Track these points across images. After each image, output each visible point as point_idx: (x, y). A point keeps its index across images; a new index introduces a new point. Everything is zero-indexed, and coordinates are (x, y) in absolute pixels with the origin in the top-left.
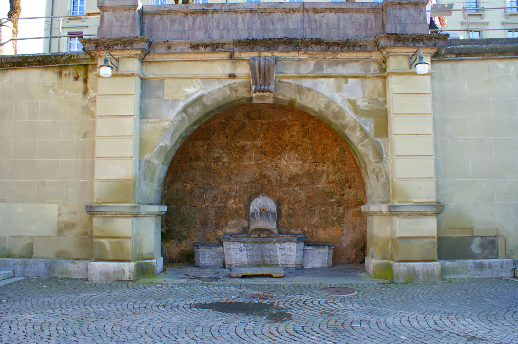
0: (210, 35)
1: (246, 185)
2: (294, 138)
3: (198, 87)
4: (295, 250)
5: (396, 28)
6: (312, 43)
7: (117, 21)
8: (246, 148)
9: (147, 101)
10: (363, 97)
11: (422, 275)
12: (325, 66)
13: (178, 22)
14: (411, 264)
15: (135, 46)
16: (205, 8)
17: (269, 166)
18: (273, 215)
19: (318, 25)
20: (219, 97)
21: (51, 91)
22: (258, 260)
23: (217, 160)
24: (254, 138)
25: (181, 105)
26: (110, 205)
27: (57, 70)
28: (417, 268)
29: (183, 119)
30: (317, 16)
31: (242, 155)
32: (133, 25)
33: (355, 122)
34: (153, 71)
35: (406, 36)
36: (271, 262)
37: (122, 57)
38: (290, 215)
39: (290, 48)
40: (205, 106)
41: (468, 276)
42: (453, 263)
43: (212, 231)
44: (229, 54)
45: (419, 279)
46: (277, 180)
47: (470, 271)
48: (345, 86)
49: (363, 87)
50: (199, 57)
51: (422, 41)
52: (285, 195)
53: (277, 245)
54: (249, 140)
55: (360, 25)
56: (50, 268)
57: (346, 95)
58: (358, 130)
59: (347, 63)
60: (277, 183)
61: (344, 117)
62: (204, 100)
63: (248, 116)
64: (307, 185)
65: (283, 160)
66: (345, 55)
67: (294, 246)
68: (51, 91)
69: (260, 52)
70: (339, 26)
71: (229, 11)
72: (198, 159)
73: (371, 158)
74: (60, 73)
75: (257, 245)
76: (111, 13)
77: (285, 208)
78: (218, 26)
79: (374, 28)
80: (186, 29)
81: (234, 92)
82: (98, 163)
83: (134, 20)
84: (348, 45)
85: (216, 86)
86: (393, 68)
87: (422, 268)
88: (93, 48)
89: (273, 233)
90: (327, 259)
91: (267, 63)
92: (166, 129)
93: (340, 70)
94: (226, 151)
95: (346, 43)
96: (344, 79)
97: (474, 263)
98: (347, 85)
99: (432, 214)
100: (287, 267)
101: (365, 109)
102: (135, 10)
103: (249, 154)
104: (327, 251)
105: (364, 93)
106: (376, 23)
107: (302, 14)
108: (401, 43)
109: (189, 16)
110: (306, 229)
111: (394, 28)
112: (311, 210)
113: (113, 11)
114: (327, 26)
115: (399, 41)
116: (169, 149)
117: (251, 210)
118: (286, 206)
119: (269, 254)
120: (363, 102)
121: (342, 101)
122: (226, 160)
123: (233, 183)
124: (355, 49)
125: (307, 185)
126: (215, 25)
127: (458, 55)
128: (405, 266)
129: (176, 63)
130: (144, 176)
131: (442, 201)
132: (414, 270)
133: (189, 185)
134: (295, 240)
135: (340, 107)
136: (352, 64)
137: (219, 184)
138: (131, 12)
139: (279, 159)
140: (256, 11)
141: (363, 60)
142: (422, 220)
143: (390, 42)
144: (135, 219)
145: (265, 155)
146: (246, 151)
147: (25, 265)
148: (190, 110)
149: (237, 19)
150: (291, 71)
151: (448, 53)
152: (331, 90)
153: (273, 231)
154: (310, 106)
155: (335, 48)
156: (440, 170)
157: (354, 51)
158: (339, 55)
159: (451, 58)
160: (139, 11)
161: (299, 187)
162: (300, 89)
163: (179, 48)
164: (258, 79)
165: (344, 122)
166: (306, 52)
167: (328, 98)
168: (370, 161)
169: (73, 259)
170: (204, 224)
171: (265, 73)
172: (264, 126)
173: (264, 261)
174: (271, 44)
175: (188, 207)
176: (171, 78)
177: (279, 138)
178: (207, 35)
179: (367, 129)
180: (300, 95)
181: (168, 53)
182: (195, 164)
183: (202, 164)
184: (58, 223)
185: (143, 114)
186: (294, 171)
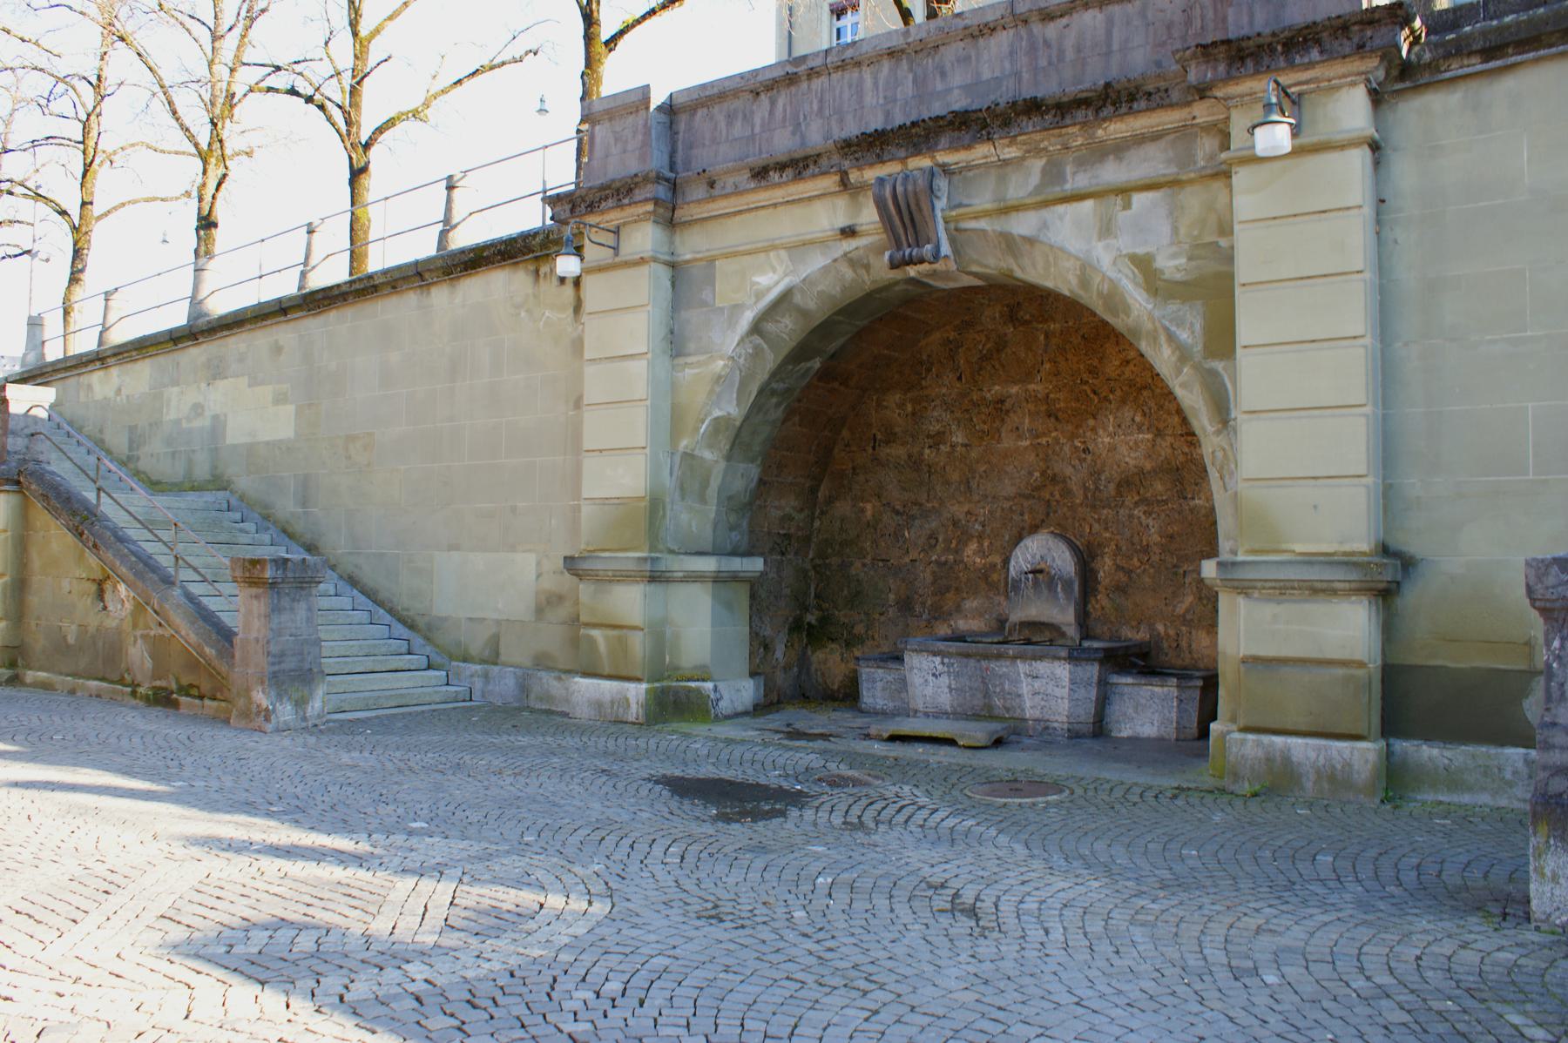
0: (803, 137)
1: (1007, 505)
2: (1131, 366)
3: (780, 270)
4: (1066, 682)
5: (1251, 16)
6: (1018, 115)
7: (616, 140)
8: (1007, 405)
9: (684, 315)
10: (1172, 244)
11: (1312, 777)
12: (1069, 169)
13: (740, 116)
14: (1279, 740)
15: (639, 195)
16: (791, 69)
17: (1066, 449)
18: (1068, 585)
19: (1054, 53)
20: (831, 286)
21: (523, 314)
22: (976, 702)
23: (938, 439)
24: (1028, 376)
25: (748, 317)
26: (607, 554)
27: (532, 268)
28: (1297, 756)
29: (757, 353)
30: (1052, 30)
31: (998, 423)
32: (645, 144)
33: (1151, 317)
34: (692, 245)
35: (1261, 40)
36: (1008, 710)
37: (624, 224)
38: (1121, 589)
39: (967, 138)
40: (803, 313)
41: (1503, 802)
42: (1448, 754)
43: (923, 624)
44: (837, 178)
45: (1302, 788)
46: (1086, 489)
47: (1510, 784)
48: (1122, 217)
49: (1174, 212)
50: (778, 194)
51: (1318, 42)
52: (1106, 529)
53: (1022, 667)
54: (1015, 383)
55: (1169, 26)
56: (524, 688)
57: (1126, 243)
58: (1165, 337)
59: (1128, 148)
60: (1086, 497)
61: (1127, 310)
62: (798, 298)
63: (1012, 316)
64: (1166, 502)
65: (1101, 432)
66: (1116, 129)
67: (1062, 670)
68: (523, 314)
69: (903, 160)
70: (1109, 45)
71: (842, 66)
72: (891, 438)
73: (1206, 422)
74: (537, 272)
75: (972, 662)
76: (607, 124)
77: (1105, 567)
78: (821, 109)
79: (1211, 25)
80: (757, 130)
81: (863, 272)
82: (590, 464)
83: (647, 132)
84: (1114, 98)
85: (816, 262)
86: (1240, 145)
87: (1312, 755)
88: (568, 213)
89: (1063, 635)
90: (1174, 715)
91: (910, 188)
92: (720, 377)
93: (1111, 173)
94: (958, 415)
95: (1107, 96)
96: (1119, 199)
97: (1528, 762)
98: (1127, 213)
99: (1358, 591)
100: (1047, 728)
101: (1179, 276)
102: (648, 108)
103: (1014, 419)
104: (1174, 692)
105: (1175, 230)
106: (1216, 11)
107: (1012, 32)
108: (1250, 63)
109: (763, 96)
110: (1160, 628)
111: (1245, 19)
112: (1176, 574)
113: (610, 119)
114: (1079, 51)
115: (1242, 59)
116: (738, 424)
117: (1012, 572)
118: (1108, 561)
119: (1003, 690)
120: (1174, 256)
121: (1114, 263)
122: (959, 438)
123: (976, 498)
124: (1135, 106)
125: (1166, 502)
126: (815, 107)
127: (1489, 53)
128: (1259, 744)
129: (738, 218)
130: (682, 488)
131: (1412, 544)
132: (1287, 760)
133: (869, 507)
134: (1064, 653)
135: (1111, 280)
136: (1140, 149)
137: (942, 503)
138: (640, 119)
139: (1094, 430)
140: (903, 51)
141: (1176, 130)
142: (1321, 610)
143: (1215, 69)
144: (651, 588)
145: (1057, 419)
146: (1008, 412)
147: (486, 676)
148: (770, 327)
149: (861, 80)
150: (983, 199)
151: (1447, 56)
152: (1086, 235)
153: (1064, 629)
154: (1049, 284)
155: (1080, 114)
156: (1388, 450)
157: (1131, 112)
158: (1100, 132)
159: (1461, 72)
160: (659, 108)
161: (1143, 508)
162: (1010, 244)
163: (730, 181)
164: (901, 231)
165: (1130, 321)
166: (1013, 141)
167: (1078, 259)
168: (1204, 429)
169: (561, 671)
170: (906, 605)
171: (910, 213)
172: (1054, 341)
173: (989, 707)
174: (918, 135)
175: (868, 561)
176: (727, 256)
177: (1093, 371)
178: (798, 137)
179: (1184, 336)
180: (1015, 257)
181: (713, 199)
182: (884, 451)
183: (898, 451)
184: (537, 593)
185: (675, 343)
186: (1132, 463)
